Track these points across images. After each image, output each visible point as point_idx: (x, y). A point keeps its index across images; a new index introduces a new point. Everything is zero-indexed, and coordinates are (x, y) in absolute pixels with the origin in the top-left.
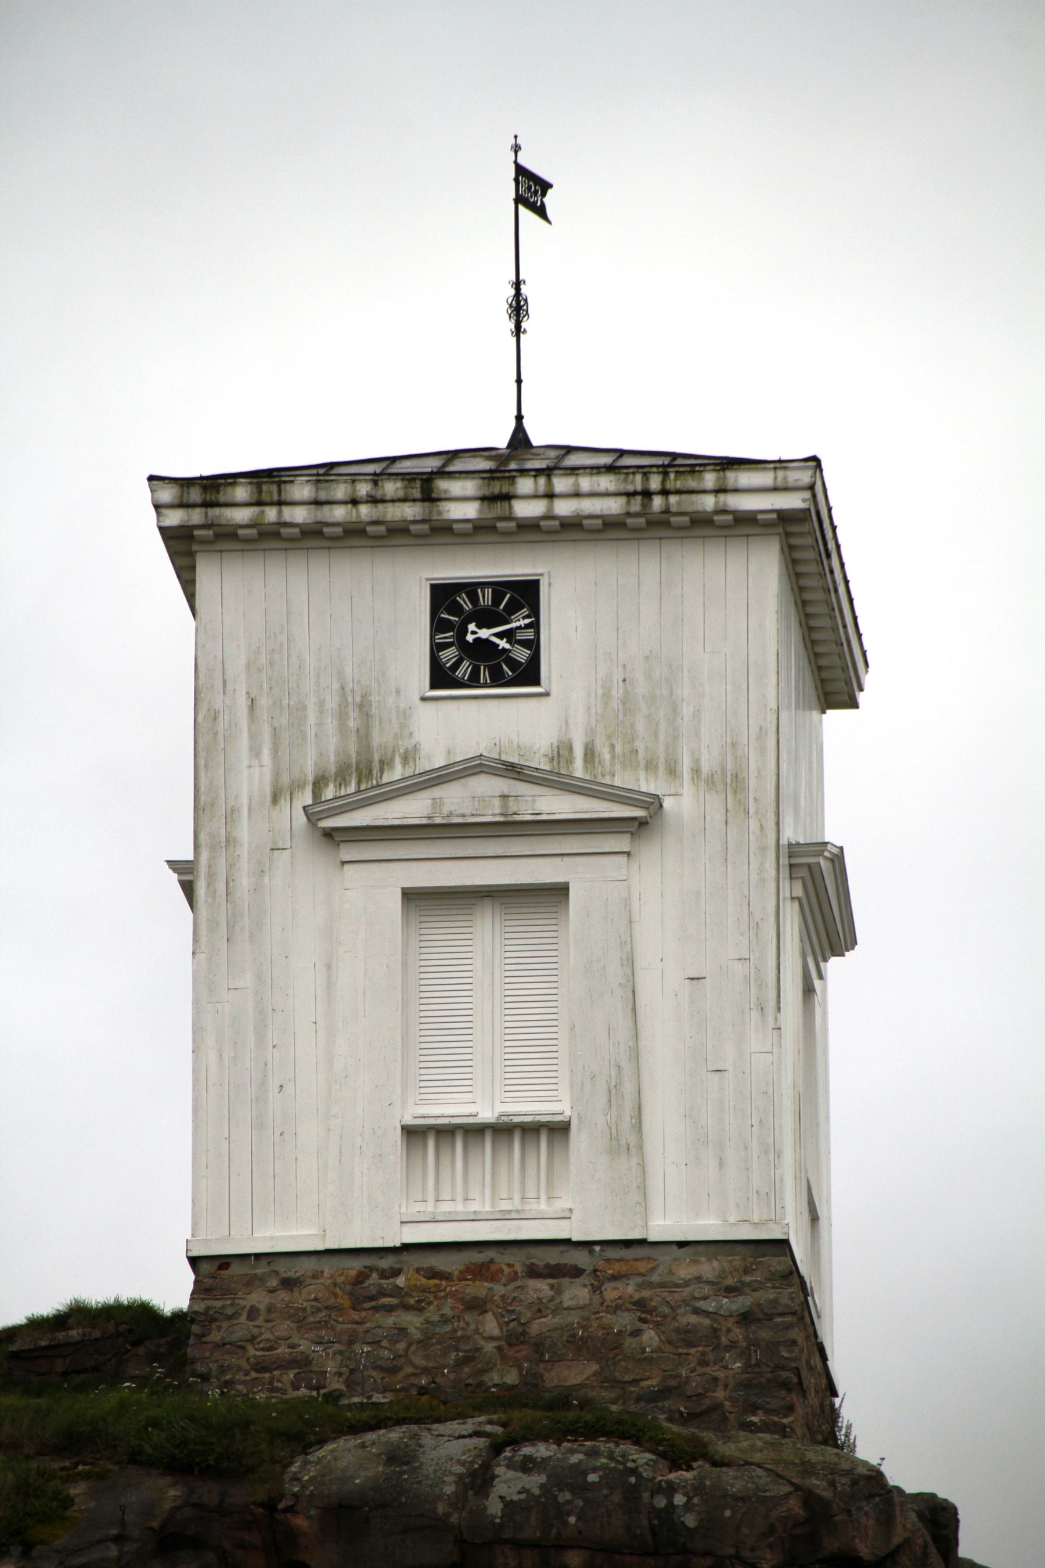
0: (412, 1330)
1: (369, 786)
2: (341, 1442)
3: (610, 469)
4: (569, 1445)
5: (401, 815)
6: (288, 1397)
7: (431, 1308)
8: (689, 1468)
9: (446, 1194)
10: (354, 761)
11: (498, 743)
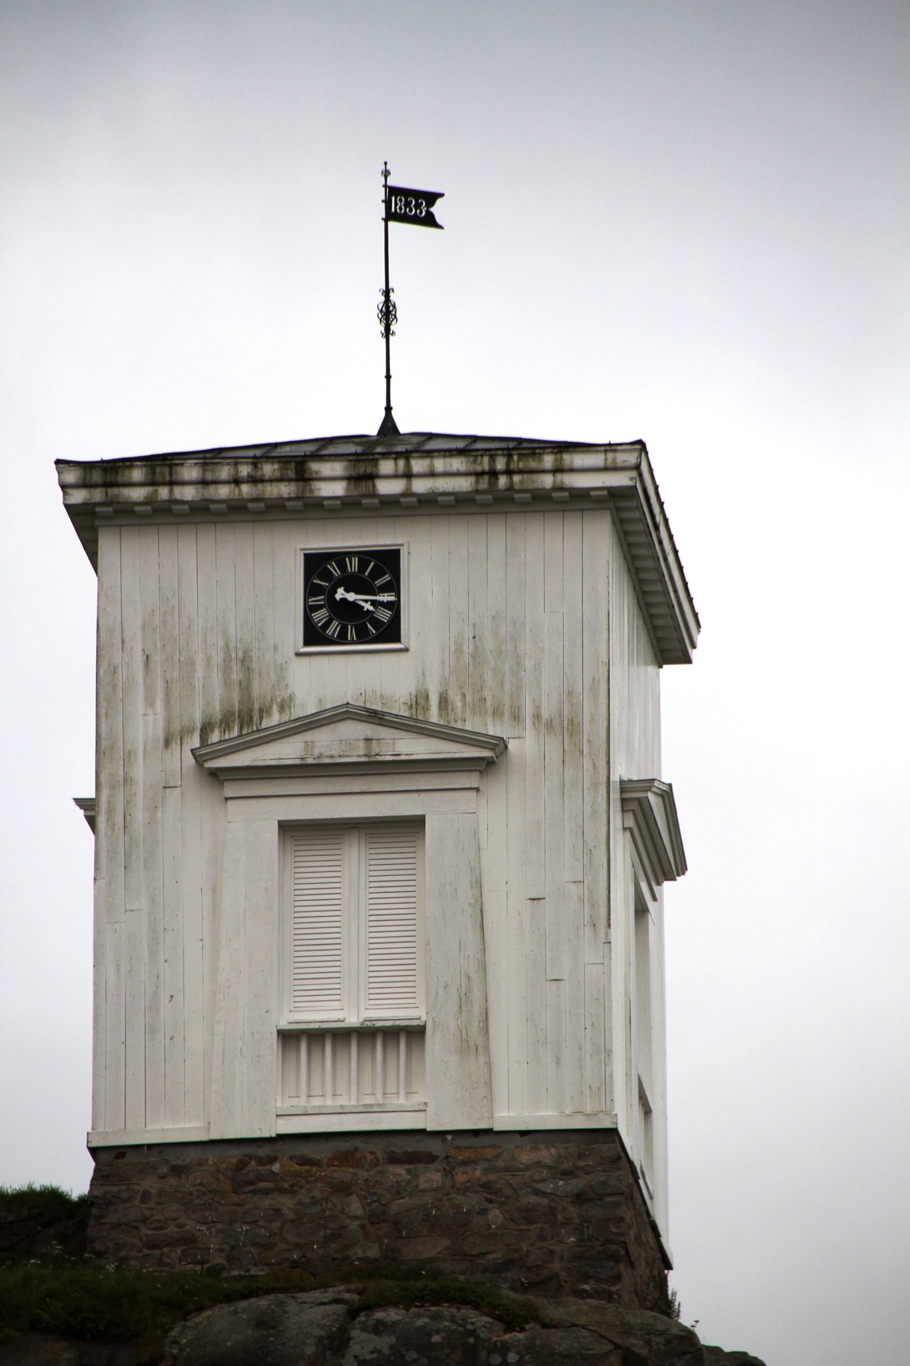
0: (285, 1211)
1: (250, 731)
2: (217, 1310)
3: (460, 452)
4: (416, 1310)
5: (277, 757)
6: (176, 1270)
7: (303, 1191)
8: (522, 1330)
9: (316, 1090)
10: (237, 709)
11: (363, 693)
